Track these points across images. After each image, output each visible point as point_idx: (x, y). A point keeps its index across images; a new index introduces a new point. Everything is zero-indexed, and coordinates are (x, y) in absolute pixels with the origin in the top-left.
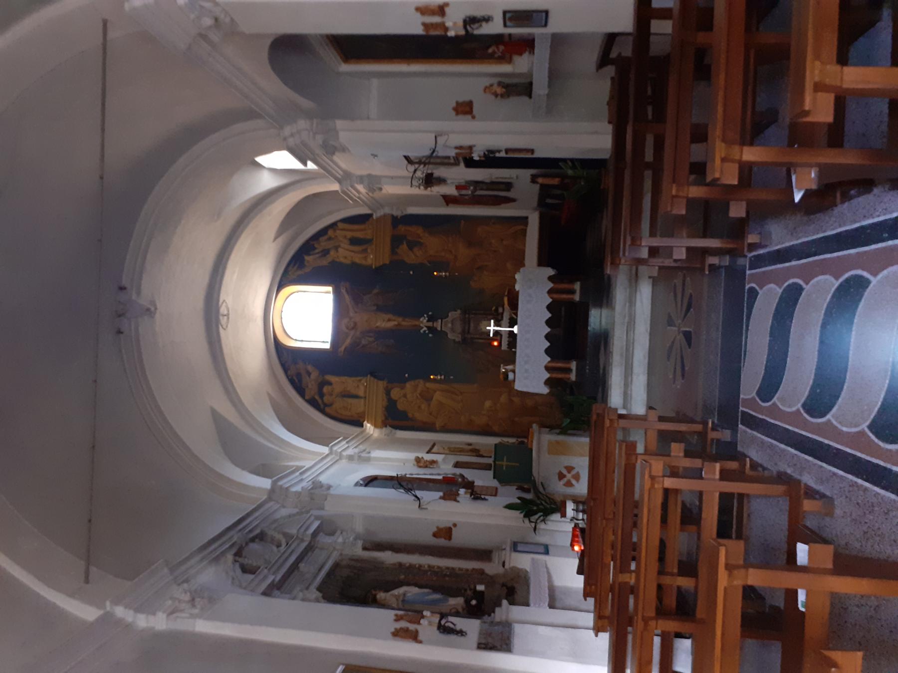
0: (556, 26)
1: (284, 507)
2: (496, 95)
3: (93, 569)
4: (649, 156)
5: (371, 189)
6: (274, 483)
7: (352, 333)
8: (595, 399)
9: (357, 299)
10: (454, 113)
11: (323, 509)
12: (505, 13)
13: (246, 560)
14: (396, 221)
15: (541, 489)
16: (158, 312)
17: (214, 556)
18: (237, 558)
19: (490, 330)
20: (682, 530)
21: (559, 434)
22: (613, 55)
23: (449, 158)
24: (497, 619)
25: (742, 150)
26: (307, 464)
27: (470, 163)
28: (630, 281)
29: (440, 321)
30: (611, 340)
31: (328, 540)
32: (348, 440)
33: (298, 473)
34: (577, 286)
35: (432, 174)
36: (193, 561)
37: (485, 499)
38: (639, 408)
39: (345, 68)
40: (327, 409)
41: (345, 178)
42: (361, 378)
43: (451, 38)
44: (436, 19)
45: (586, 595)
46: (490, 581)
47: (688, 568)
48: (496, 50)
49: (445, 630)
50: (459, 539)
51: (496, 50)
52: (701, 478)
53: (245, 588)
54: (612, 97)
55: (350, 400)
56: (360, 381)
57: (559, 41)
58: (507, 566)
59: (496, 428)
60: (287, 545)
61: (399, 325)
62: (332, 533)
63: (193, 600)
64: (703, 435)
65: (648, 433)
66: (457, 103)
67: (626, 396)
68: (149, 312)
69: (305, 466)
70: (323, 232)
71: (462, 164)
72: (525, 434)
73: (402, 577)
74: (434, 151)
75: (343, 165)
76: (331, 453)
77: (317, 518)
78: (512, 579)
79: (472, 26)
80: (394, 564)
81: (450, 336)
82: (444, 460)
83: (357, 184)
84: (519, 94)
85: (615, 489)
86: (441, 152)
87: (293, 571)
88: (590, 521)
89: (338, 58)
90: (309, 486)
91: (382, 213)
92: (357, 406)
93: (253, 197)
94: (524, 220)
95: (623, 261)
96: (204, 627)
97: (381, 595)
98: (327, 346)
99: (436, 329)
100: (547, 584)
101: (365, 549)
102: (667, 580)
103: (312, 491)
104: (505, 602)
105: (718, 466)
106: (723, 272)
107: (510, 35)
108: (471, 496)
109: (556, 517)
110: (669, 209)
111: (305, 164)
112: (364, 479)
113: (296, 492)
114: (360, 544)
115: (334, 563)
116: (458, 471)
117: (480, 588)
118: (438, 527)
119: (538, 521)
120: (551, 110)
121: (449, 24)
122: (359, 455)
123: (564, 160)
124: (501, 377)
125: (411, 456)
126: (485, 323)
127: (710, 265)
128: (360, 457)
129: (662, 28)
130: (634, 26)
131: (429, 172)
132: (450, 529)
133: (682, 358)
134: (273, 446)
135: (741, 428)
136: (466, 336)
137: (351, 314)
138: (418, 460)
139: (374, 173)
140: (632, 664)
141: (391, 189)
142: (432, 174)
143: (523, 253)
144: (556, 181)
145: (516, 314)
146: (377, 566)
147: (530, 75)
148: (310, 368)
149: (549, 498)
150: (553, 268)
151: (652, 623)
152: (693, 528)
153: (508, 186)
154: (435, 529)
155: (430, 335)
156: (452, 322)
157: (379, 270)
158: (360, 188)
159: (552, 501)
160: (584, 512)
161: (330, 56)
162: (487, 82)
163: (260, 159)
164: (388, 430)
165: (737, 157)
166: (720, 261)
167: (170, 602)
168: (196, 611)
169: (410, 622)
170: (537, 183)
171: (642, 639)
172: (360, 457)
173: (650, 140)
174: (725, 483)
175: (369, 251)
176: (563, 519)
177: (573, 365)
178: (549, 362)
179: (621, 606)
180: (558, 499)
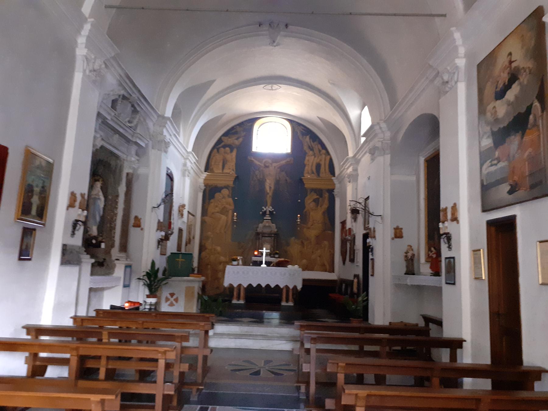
0: (447, 289)
1: (154, 125)
2: (406, 253)
3: (114, 10)
4: (367, 348)
5: (350, 176)
6: (168, 118)
7: (263, 165)
8: (221, 315)
9: (282, 168)
10: (395, 227)
11: (153, 148)
12: (453, 258)
13: (120, 102)
14: (331, 192)
15: (165, 282)
16: (273, 47)
17: (122, 82)
18: (121, 97)
19: (263, 250)
20: (136, 371)
21: (198, 294)
22: (430, 324)
23: (368, 224)
24: (82, 256)
25: (363, 407)
26: (181, 139)
27: (366, 237)
28: (294, 337)
29: (270, 218)
30: (256, 325)
31: (133, 152)
32: (196, 163)
33: (175, 133)
34: (291, 304)
35: (359, 213)
36: (120, 71)
37: (158, 247)
38: (213, 343)
39: (422, 160)
40: (215, 150)
41: (356, 161)
42: (235, 171)
43: (438, 225)
44: (449, 216)
45: (98, 311)
46: (108, 252)
47: (111, 375)
48: (433, 253)
49: (75, 224)
50: (133, 232)
51: (433, 253)
52: (165, 382)
53: (102, 102)
54: (406, 325)
55: (221, 164)
56: (233, 170)
57: (438, 290)
58: (116, 262)
59: (203, 254)
60: (130, 127)
61: (268, 194)
62: (137, 154)
63: (94, 71)
64: (195, 383)
65: (196, 349)
66: (402, 229)
67: (222, 335)
68: (273, 42)
69: (179, 136)
71: (365, 232)
72: (200, 272)
73: (110, 197)
74: (372, 214)
75: (363, 159)
76: (188, 153)
77: (147, 145)
78: (107, 265)
79: (446, 238)
80: (118, 192)
81: (261, 225)
82: (184, 222)
83: (353, 167)
84: (407, 267)
85: (163, 329)
86: (372, 219)
87: (114, 131)
88: (144, 314)
89: (428, 156)
90: (166, 140)
91: (335, 183)
92: (218, 170)
93: (343, 104)
94: (332, 270)
95: (302, 332)
96: (78, 78)
97: (98, 185)
98: (254, 149)
99: (265, 216)
100: (105, 286)
101: (128, 174)
102: (103, 361)
103: (163, 142)
104: (93, 261)
105: (172, 393)
106: (296, 395)
107: (441, 261)
108: (160, 239)
109: (147, 292)
110: (330, 361)
111: (364, 136)
112: (171, 173)
113: (163, 132)
114: (131, 171)
115: (118, 155)
116: (176, 232)
117: (103, 245)
118: (141, 219)
119: (144, 281)
120: (399, 286)
121: (446, 224)
122: (187, 170)
123: (367, 295)
124: (235, 257)
125: (186, 202)
126: (269, 246)
127: (300, 386)
128: (185, 170)
129: (444, 355)
130: (447, 338)
131: (360, 212)
133: (242, 370)
134: (191, 119)
135: (198, 407)
136: (261, 235)
137: (274, 164)
138: (183, 206)
139: (359, 178)
140: (52, 340)
141: (350, 188)
142: (359, 213)
143: (312, 269)
144: (355, 290)
145: (273, 266)
146: (118, 182)
147: (419, 274)
148: (241, 140)
149: (158, 287)
150: (302, 288)
151: (75, 353)
152: (137, 377)
153: (352, 260)
154: (140, 217)
155: (261, 213)
156: (269, 226)
157: (301, 181)
158: (350, 169)
159: (156, 290)
160: (150, 309)
161: (428, 152)
162: (415, 247)
163: (366, 108)
164: (203, 187)
165: (358, 404)
166: (303, 393)
167: (93, 57)
168: (87, 72)
169: (80, 203)
170: (354, 278)
171: (65, 346)
172: (185, 170)
173: (376, 348)
174: (161, 397)
175: (312, 175)
176: (145, 296)
177: (242, 302)
178: (243, 286)
179: (90, 333)
180: (158, 294)
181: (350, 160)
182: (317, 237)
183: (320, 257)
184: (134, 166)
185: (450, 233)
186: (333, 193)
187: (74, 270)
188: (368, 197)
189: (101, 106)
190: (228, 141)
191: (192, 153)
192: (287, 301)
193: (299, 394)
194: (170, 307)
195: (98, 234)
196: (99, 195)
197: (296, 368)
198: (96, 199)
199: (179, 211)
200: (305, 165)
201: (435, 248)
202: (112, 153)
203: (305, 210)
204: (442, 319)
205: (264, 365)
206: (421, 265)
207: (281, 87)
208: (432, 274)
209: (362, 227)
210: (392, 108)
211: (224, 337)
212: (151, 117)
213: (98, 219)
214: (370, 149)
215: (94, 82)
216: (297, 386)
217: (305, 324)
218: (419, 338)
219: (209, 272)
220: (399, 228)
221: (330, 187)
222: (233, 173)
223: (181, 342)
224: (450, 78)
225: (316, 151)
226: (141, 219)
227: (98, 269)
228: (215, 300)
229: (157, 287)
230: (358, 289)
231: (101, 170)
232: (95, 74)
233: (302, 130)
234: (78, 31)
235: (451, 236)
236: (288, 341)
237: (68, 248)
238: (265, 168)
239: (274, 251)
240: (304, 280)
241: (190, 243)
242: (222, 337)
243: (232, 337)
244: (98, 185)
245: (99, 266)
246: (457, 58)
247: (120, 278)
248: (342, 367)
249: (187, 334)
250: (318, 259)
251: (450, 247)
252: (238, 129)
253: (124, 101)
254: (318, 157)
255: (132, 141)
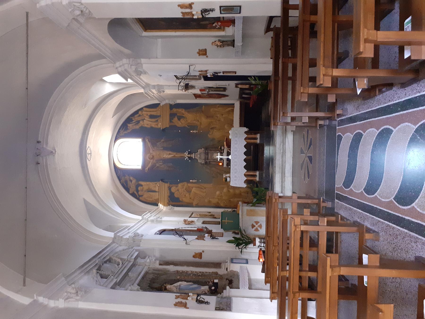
0: (244, 13)
1: (120, 246)
3: (27, 279)
4: (290, 74)
6: (115, 234)
7: (152, 161)
9: (154, 144)
10: (198, 55)
11: (139, 246)
12: (220, 7)
14: (171, 107)
15: (244, 233)
18: (98, 271)
20: (310, 250)
21: (252, 206)
22: (272, 27)
23: (196, 76)
24: (224, 295)
26: (132, 225)
27: (206, 78)
29: (194, 154)
33: (127, 229)
34: (258, 136)
36: (76, 274)
37: (217, 239)
38: (288, 193)
39: (145, 34)
40: (140, 198)
41: (147, 86)
44: (188, 10)
45: (266, 282)
46: (221, 277)
47: (313, 268)
48: (217, 25)
50: (205, 258)
51: (217, 25)
52: (318, 225)
54: (272, 46)
55: (151, 193)
56: (156, 184)
57: (246, 20)
58: (228, 270)
59: (222, 205)
61: (174, 156)
62: (144, 258)
64: (318, 205)
65: (293, 205)
67: (283, 187)
68: (52, 153)
70: (136, 112)
71: (202, 79)
72: (236, 207)
75: (146, 81)
76: (143, 219)
82: (197, 220)
84: (228, 45)
86: (192, 73)
88: (267, 247)
89: (142, 29)
91: (165, 103)
92: (155, 196)
96: (82, 305)
97: (168, 287)
98: (140, 167)
102: (303, 274)
103: (134, 238)
104: (228, 287)
109: (251, 246)
112: (159, 231)
113: (126, 238)
114: (158, 262)
116: (204, 226)
117: (216, 281)
119: (243, 248)
120: (243, 53)
123: (250, 77)
124: (224, 180)
126: (215, 154)
127: (320, 125)
128: (157, 220)
132: (201, 253)
136: (207, 161)
137: (151, 152)
138: (185, 221)
139: (160, 84)
141: (168, 91)
144: (247, 86)
145: (230, 150)
146: (166, 272)
147: (233, 36)
151: (297, 295)
152: (315, 249)
153: (225, 89)
155: (190, 161)
158: (154, 91)
160: (264, 243)
161: (138, 28)
162: (213, 40)
164: (171, 207)
165: (330, 74)
168: (78, 298)
170: (238, 87)
172: (157, 220)
173: (290, 66)
175: (159, 121)
177: (257, 173)
178: (246, 172)
179: (282, 287)
180: (252, 237)
181: (146, 91)
182: (207, 117)
183: (222, 115)
184: (154, 260)
185: (201, 9)
186: (173, 105)
187: (234, 300)
188: (175, 76)
189: (106, 287)
190: (133, 189)
191: (143, 216)
192: (256, 139)
193: (325, 125)
194: (262, 228)
195: (208, 285)
196: (177, 286)
197: (306, 129)
198: (179, 288)
199: (189, 224)
200: (152, 128)
201: (214, 23)
202: (143, 278)
203: (187, 127)
204: (268, 16)
205: (305, 154)
206: (227, 35)
207: (89, 147)
208: (233, 26)
209: (199, 81)
210: (104, 58)
211: (284, 185)
212: (114, 248)
213: (196, 286)
214: (137, 75)
215: (86, 292)
216: (319, 128)
217: (273, 122)
218: (281, 36)
219: (236, 200)
220: (199, 52)
221: (168, 107)
222: (159, 184)
223: (288, 215)
224: (78, 9)
225: (139, 118)
226: (195, 253)
227: (234, 284)
228: (257, 193)
229: (247, 238)
230: (246, 84)
231: (156, 285)
232: (80, 292)
233: (124, 129)
234: (45, 307)
235: (203, 9)
236: (286, 137)
237: (218, 306)
238: (154, 159)
239: (219, 150)
240: (241, 126)
241: (214, 215)
242: (284, 187)
243: (284, 180)
244: (168, 287)
245: (232, 283)
246: (62, 3)
247: (241, 267)
248: (303, 90)
249: (282, 210)
250: (224, 116)
251: (212, 10)
252: (123, 180)
253: (102, 269)
254: (145, 117)
255: (134, 262)
